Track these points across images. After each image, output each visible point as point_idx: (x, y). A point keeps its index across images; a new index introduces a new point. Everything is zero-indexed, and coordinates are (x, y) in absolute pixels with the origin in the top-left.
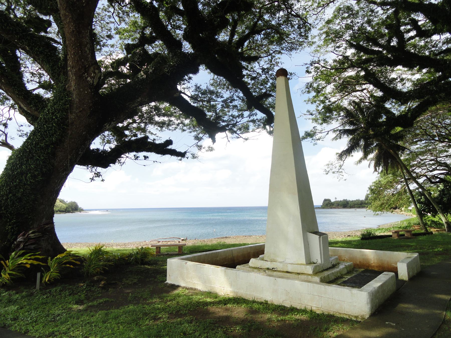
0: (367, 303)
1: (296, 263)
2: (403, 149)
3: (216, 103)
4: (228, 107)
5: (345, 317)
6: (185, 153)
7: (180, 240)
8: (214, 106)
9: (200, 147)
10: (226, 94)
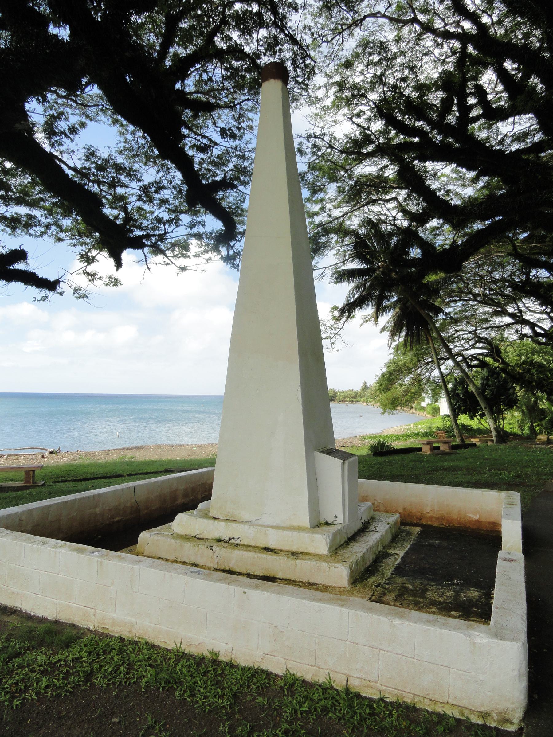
0: (520, 676)
1: (288, 524)
2: (438, 310)
3: (127, 190)
4: (150, 200)
5: (449, 712)
6: (57, 282)
7: (46, 453)
8: (123, 198)
9: (92, 276)
10: (150, 174)
